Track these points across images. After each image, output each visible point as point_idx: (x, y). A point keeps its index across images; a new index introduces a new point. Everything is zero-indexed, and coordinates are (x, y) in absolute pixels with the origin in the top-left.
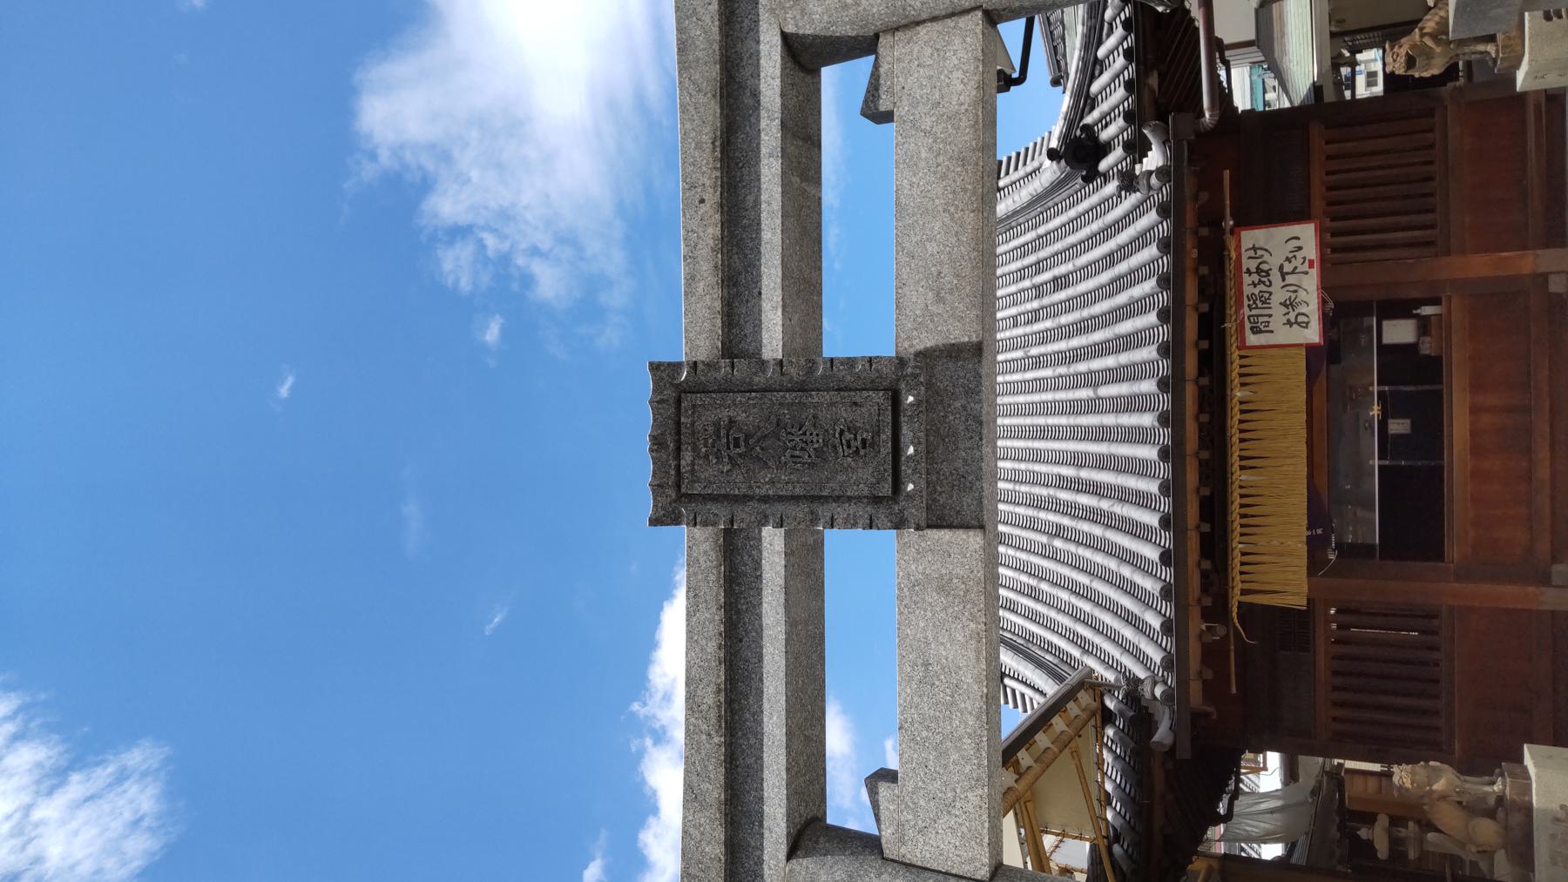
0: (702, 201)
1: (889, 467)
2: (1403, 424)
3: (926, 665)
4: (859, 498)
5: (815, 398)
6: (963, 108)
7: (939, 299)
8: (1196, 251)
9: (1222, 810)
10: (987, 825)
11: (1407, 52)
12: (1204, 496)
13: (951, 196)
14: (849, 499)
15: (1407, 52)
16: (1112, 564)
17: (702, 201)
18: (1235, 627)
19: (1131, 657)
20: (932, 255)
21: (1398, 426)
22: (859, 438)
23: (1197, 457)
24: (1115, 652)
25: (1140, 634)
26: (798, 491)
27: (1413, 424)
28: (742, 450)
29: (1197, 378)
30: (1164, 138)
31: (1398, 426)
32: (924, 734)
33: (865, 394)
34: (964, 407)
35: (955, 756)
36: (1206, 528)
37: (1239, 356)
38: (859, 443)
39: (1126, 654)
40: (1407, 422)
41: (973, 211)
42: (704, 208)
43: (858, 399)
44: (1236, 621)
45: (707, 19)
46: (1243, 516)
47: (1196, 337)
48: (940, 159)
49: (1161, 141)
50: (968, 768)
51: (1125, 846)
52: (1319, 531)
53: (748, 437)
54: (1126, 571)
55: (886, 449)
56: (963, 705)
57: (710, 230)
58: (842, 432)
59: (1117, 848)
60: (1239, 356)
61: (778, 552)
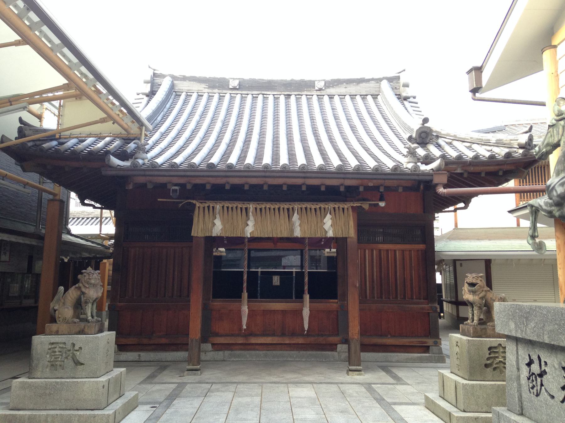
2: (277, 282)
8: (372, 185)
11: (478, 284)
12: (340, 188)
15: (478, 284)
18: (183, 202)
19: (191, 153)
21: (276, 280)
23: (265, 184)
27: (277, 286)
29: (306, 184)
30: (434, 170)
31: (276, 280)
36: (227, 187)
37: (289, 208)
39: (161, 150)
44: (186, 202)
46: (279, 209)
47: (327, 184)
51: (56, 147)
52: (225, 242)
59: (54, 143)
60: (289, 208)
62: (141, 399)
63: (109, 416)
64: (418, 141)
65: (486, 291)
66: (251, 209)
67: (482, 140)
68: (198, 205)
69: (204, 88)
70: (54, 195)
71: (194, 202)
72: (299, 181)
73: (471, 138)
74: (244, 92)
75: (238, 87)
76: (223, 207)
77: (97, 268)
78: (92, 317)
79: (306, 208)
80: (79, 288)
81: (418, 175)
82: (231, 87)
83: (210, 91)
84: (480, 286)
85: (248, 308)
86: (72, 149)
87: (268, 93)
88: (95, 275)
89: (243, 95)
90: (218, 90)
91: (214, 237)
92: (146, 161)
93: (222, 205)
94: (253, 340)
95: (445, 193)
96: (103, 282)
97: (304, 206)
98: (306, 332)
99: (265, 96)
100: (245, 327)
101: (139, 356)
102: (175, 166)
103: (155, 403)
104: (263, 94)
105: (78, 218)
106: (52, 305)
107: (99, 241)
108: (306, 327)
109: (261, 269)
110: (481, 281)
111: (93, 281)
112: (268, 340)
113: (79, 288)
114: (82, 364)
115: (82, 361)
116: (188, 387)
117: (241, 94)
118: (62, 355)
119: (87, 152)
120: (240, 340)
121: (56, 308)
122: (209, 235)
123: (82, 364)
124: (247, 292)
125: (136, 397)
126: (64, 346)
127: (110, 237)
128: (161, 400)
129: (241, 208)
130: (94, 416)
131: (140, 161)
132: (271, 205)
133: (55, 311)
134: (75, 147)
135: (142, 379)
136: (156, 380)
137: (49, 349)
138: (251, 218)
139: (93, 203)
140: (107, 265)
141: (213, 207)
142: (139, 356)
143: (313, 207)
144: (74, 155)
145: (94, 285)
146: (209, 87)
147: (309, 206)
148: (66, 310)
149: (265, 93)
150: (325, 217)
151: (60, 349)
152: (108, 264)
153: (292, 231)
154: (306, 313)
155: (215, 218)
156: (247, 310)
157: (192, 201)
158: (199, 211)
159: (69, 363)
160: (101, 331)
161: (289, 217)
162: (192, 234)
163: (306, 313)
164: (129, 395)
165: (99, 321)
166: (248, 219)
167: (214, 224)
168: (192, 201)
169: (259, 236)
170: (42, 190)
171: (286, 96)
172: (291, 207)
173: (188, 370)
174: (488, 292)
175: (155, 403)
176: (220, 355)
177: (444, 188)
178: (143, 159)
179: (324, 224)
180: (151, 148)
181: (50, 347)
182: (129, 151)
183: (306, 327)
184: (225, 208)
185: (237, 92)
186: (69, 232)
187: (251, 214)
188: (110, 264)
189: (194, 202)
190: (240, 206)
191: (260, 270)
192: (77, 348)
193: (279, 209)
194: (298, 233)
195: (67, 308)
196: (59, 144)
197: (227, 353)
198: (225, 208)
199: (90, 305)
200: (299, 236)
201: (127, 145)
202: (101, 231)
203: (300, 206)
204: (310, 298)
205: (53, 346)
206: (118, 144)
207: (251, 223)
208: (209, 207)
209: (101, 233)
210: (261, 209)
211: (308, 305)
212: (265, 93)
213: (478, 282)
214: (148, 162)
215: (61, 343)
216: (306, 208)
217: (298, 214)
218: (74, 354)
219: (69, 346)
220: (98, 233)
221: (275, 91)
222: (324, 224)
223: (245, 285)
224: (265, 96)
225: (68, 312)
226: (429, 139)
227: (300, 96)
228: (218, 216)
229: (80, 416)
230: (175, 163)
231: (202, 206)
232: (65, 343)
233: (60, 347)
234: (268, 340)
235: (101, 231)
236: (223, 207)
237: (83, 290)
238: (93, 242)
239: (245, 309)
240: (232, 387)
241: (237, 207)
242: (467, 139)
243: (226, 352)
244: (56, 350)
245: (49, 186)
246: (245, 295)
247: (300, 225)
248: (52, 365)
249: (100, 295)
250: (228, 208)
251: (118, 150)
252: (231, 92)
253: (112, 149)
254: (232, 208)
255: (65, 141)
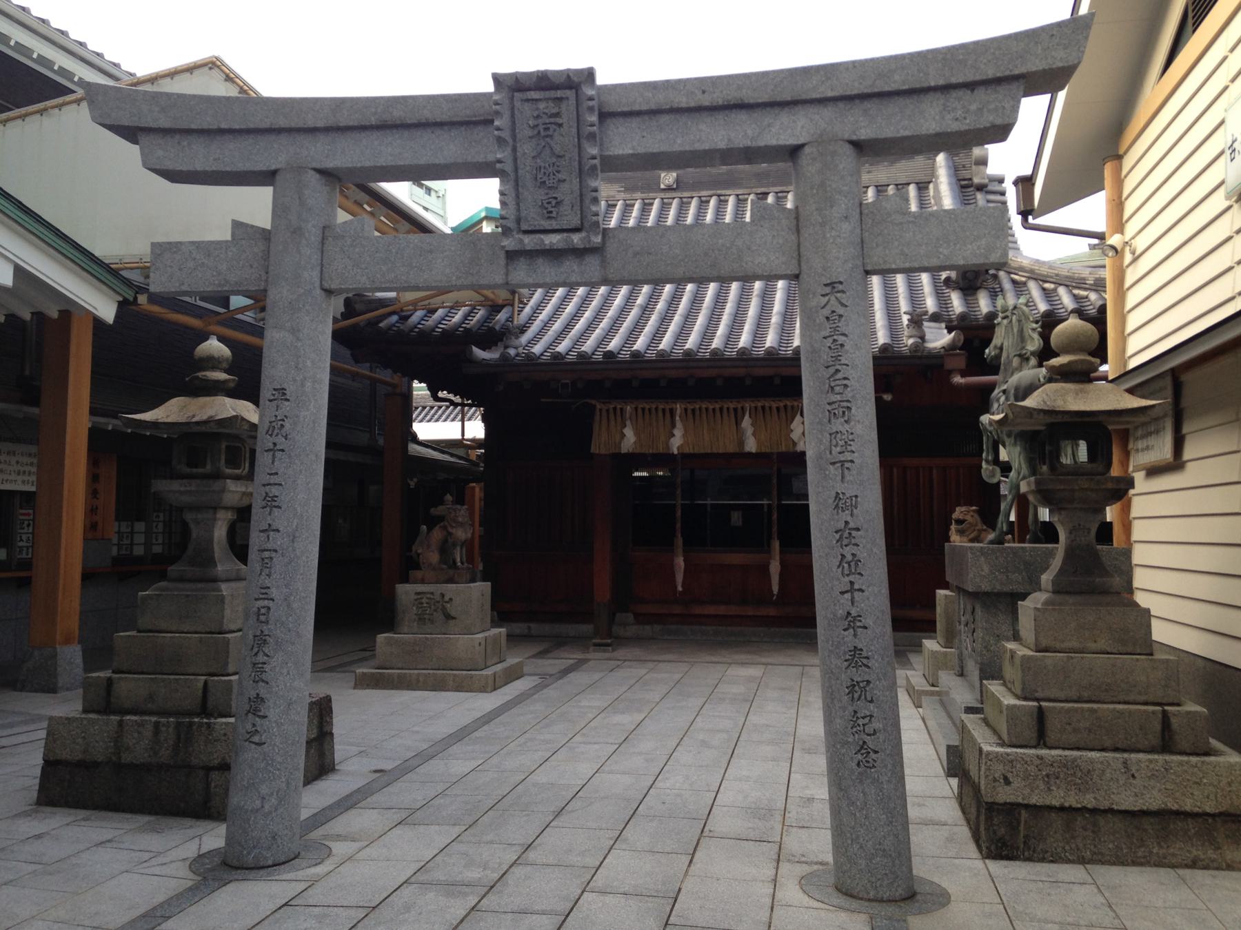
0: (704, 92)
1: (537, 228)
3: (431, 252)
4: (518, 210)
5: (576, 181)
6: (744, 264)
7: (636, 254)
9: (440, 394)
10: (351, 287)
13: (694, 259)
14: (518, 204)
16: (611, 313)
17: (704, 92)
20: (661, 249)
21: (736, 518)
22: (553, 209)
24: (543, 316)
25: (556, 336)
26: (520, 172)
28: (543, 133)
31: (736, 518)
32: (394, 251)
33: (579, 212)
34: (573, 271)
35: (384, 268)
38: (550, 209)
40: (740, 523)
41: (684, 273)
42: (699, 93)
43: (575, 208)
44: (585, 401)
45: (822, 89)
46: (721, 409)
48: (716, 252)
49: (945, 345)
50: (379, 276)
53: (551, 136)
54: (605, 324)
55: (546, 224)
56: (411, 273)
57: (684, 100)
58: (556, 198)
59: (395, 318)
61: (486, 157)
62: (526, 670)
63: (487, 676)
64: (961, 286)
65: (978, 530)
66: (678, 412)
67: (1074, 279)
68: (598, 406)
69: (619, 191)
70: (394, 386)
71: (593, 402)
72: (741, 372)
73: (1057, 275)
74: (686, 194)
75: (675, 186)
76: (636, 409)
77: (460, 500)
78: (462, 563)
79: (763, 408)
80: (445, 528)
81: (920, 358)
82: (662, 186)
83: (628, 196)
84: (970, 523)
85: (684, 560)
86: (420, 326)
87: (728, 192)
88: (462, 511)
89: (685, 200)
90: (642, 193)
91: (625, 454)
92: (521, 350)
93: (634, 406)
94: (698, 610)
95: (961, 383)
96: (474, 522)
97: (760, 404)
98: (775, 598)
99: (722, 198)
100: (680, 588)
101: (529, 628)
102: (560, 357)
103: (545, 675)
104: (719, 196)
105: (424, 408)
106: (414, 548)
107: (461, 452)
108: (775, 589)
109: (711, 500)
110: (972, 516)
111: (460, 519)
112: (722, 610)
113: (445, 528)
114: (454, 618)
115: (453, 613)
116: (591, 663)
117: (681, 198)
118: (430, 608)
119: (440, 330)
120: (677, 610)
121: (419, 551)
122: (617, 451)
123: (454, 618)
124: (682, 536)
125: (520, 665)
126: (432, 597)
127: (476, 443)
128: (554, 673)
129: (664, 410)
130: (472, 677)
131: (512, 352)
132: (709, 404)
133: (419, 555)
134: (423, 322)
135: (531, 654)
136: (549, 655)
137: (416, 600)
138: (679, 424)
139: (451, 396)
140: (477, 490)
141: (622, 409)
142: (529, 628)
143: (774, 405)
144: (425, 337)
145: (462, 525)
146: (627, 190)
147: (767, 405)
148: (431, 553)
149: (723, 192)
150: (792, 422)
151: (427, 601)
152: (477, 490)
153: (741, 443)
154: (775, 568)
155: (625, 426)
156: (682, 564)
157: (589, 401)
158: (601, 415)
159: (439, 616)
160: (473, 580)
161: (738, 423)
162: (592, 451)
163: (775, 568)
164: (512, 661)
165: (469, 569)
166: (673, 426)
167: (623, 436)
168: (589, 401)
169: (692, 451)
170: (374, 381)
171: (761, 196)
172: (739, 406)
173: (595, 645)
174: (984, 533)
175: (545, 675)
176: (647, 630)
177: (962, 376)
178: (516, 348)
179: (792, 431)
180: (530, 320)
181: (416, 597)
182: (497, 328)
183: (775, 589)
184: (640, 411)
185: (674, 195)
186: (414, 438)
187: (677, 418)
188: (480, 489)
189: (593, 402)
190: (661, 407)
191: (709, 502)
192: (447, 598)
193: (721, 409)
194: (751, 446)
195: (433, 552)
196: (400, 319)
197: (657, 628)
198: (640, 411)
199: (458, 548)
200: (754, 451)
201: (495, 314)
202: (463, 434)
203: (753, 405)
204: (780, 546)
205: (419, 597)
206: (482, 316)
207: (678, 432)
208: (615, 409)
209: (463, 439)
210: (693, 410)
211: (778, 558)
212: (723, 192)
213: (968, 518)
214: (524, 349)
215: (428, 593)
216: (763, 408)
217: (750, 417)
218: (443, 606)
219: (438, 597)
220: (459, 437)
221: (739, 188)
222: (792, 431)
223: (679, 525)
224: (722, 198)
225: (434, 557)
226: (980, 281)
227: (785, 194)
228: (628, 423)
229: (455, 675)
230: (558, 353)
231: (605, 408)
232: (432, 593)
233: (427, 598)
234: (722, 610)
235: (463, 434)
236: (636, 409)
237: (450, 530)
238: (452, 455)
239: (680, 562)
240: (651, 665)
241: (656, 409)
242: (1052, 277)
243: (655, 626)
244: (423, 601)
245: (385, 375)
246: (679, 541)
247: (754, 434)
248: (420, 619)
249: (469, 535)
250: (643, 409)
251: (482, 326)
252: (662, 195)
253: (474, 325)
254: (650, 410)
255: (409, 313)
